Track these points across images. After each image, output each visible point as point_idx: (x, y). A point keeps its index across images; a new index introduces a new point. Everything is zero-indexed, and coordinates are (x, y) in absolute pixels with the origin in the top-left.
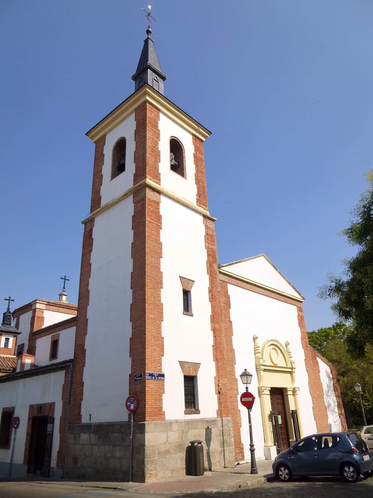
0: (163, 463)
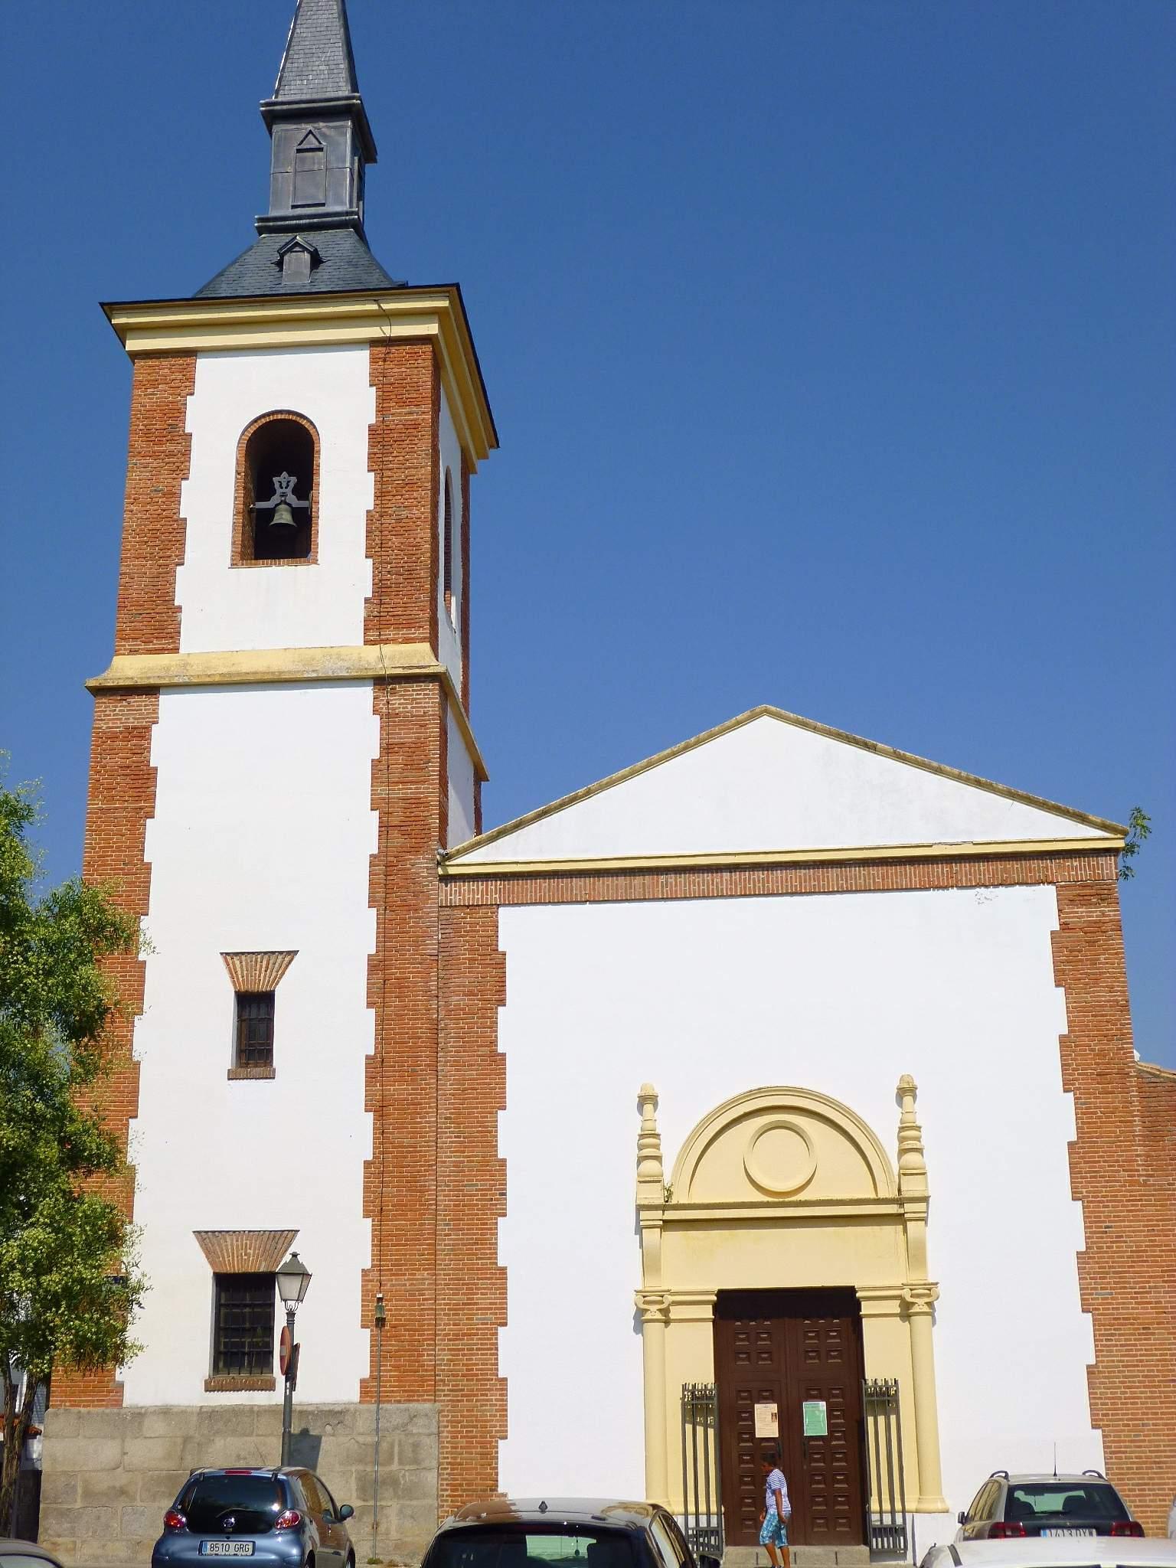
0: (103, 1519)
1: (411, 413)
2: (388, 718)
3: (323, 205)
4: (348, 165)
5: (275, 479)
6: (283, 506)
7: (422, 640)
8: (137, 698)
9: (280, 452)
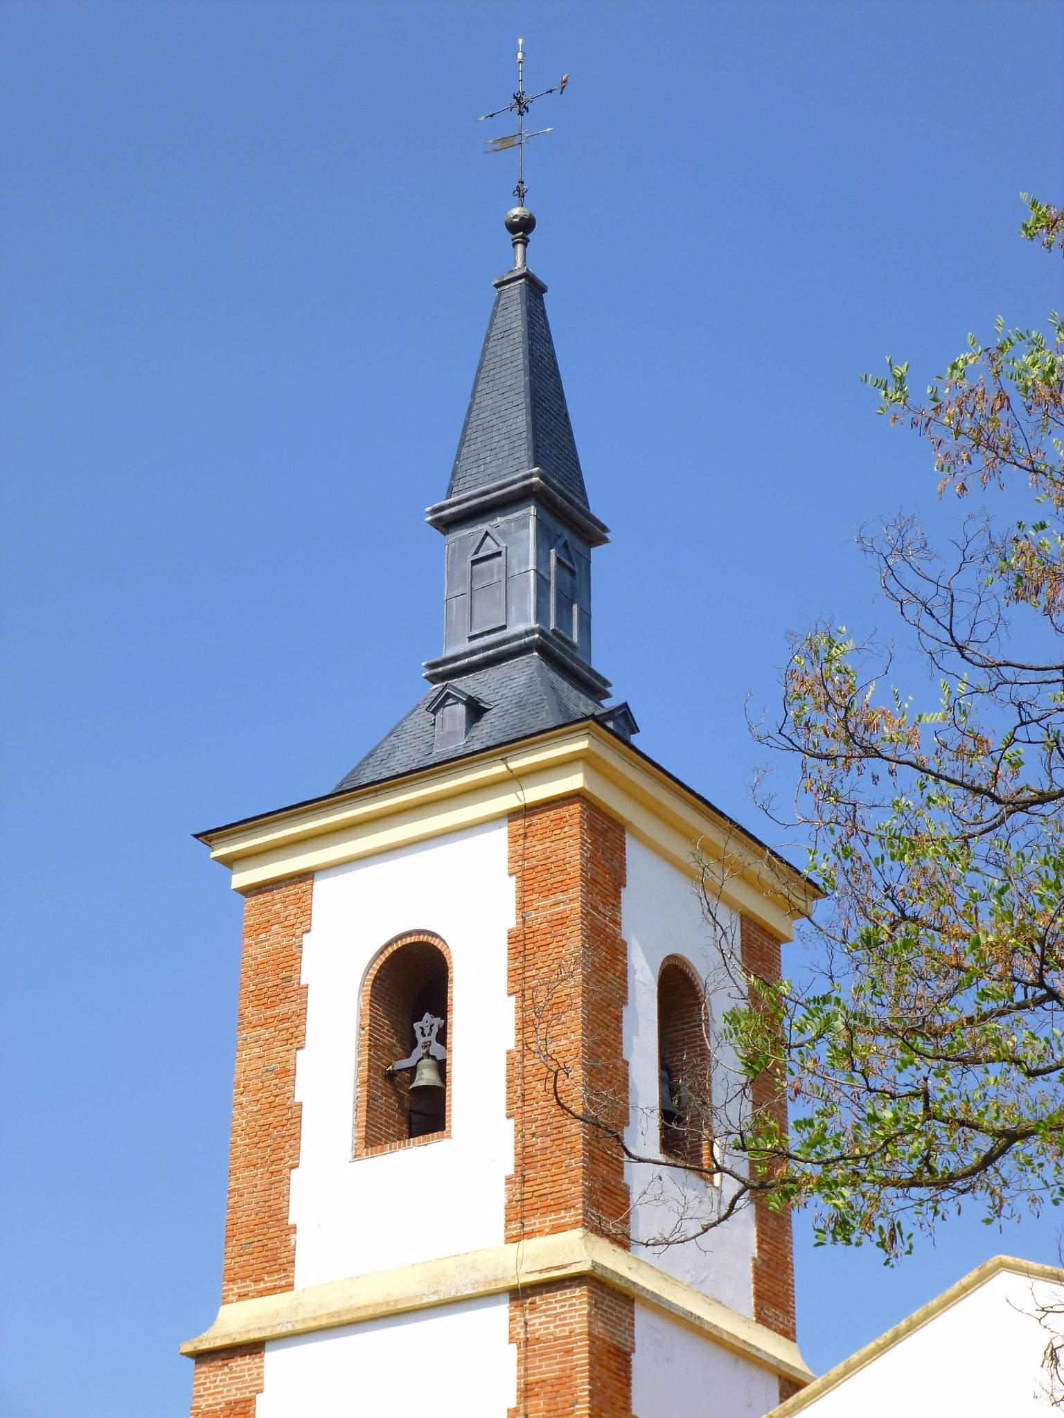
1: (557, 904)
2: (527, 1345)
3: (504, 627)
4: (532, 566)
5: (417, 1025)
6: (426, 1061)
7: (574, 1226)
8: (239, 1361)
9: (412, 983)
